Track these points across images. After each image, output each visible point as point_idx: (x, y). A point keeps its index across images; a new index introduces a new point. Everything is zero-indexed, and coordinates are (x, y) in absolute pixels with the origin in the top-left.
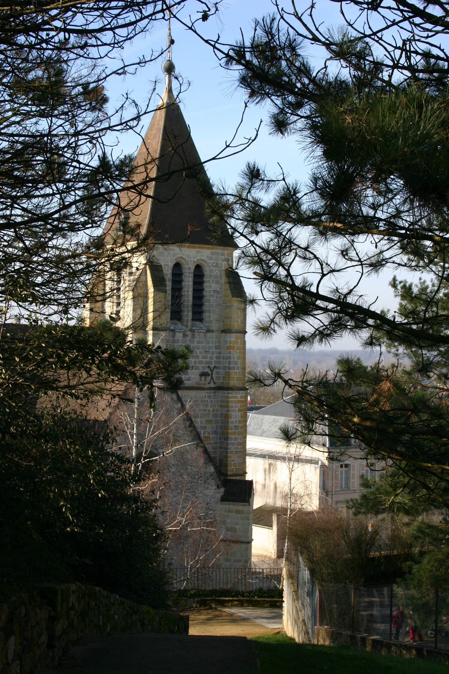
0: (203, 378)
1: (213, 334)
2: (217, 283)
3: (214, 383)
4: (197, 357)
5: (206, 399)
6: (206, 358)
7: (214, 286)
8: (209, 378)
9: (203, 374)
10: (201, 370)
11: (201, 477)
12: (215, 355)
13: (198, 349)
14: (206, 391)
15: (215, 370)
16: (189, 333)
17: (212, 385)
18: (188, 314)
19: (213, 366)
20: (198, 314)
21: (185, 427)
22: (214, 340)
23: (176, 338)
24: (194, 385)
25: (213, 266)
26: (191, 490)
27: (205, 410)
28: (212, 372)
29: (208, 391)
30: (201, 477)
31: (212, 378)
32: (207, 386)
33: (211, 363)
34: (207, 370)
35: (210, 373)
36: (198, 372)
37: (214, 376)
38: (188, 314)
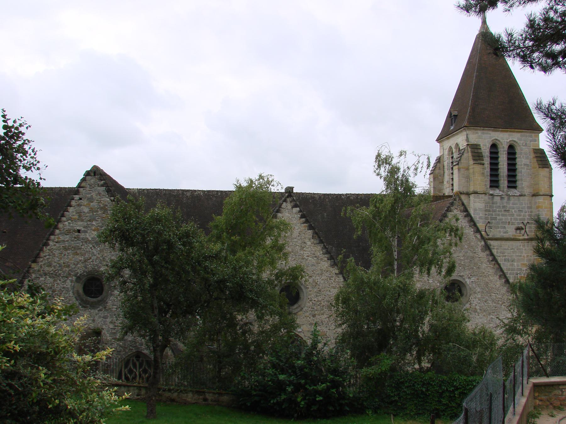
0: (518, 231)
1: (525, 197)
2: (527, 158)
4: (513, 215)
5: (521, 247)
6: (520, 216)
7: (524, 161)
8: (523, 232)
10: (517, 226)
11: (504, 303)
12: (527, 213)
13: (514, 209)
15: (528, 225)
17: (526, 237)
18: (504, 182)
19: (526, 222)
20: (512, 182)
21: (488, 261)
22: (526, 202)
23: (495, 200)
24: (511, 237)
25: (523, 145)
26: (495, 314)
27: (521, 256)
30: (504, 303)
32: (521, 238)
33: (524, 219)
35: (524, 227)
36: (514, 227)
37: (527, 229)
38: (504, 182)
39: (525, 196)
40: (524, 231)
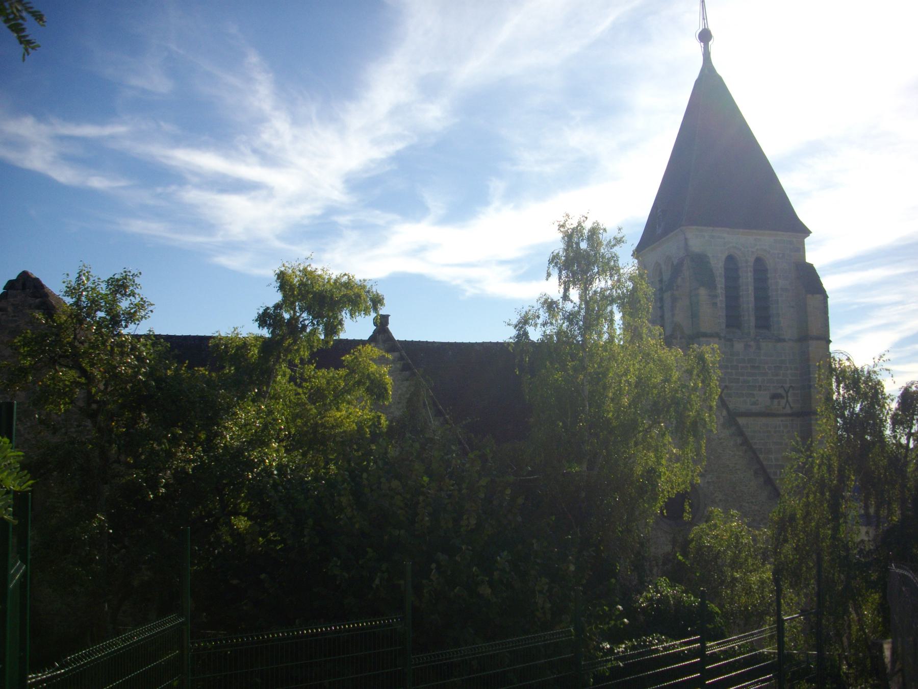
0: (776, 401)
3: (791, 408)
8: (783, 402)
9: (775, 396)
12: (789, 372)
14: (780, 419)
16: (752, 343)
17: (788, 410)
19: (788, 385)
28: (787, 393)
29: (783, 418)
31: (787, 401)
34: (781, 391)
35: (784, 395)
37: (790, 399)
39: (784, 340)
40: (785, 400)
